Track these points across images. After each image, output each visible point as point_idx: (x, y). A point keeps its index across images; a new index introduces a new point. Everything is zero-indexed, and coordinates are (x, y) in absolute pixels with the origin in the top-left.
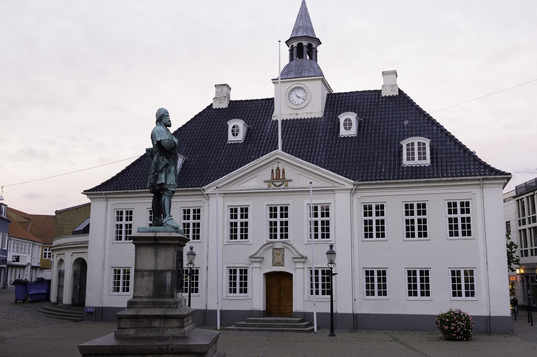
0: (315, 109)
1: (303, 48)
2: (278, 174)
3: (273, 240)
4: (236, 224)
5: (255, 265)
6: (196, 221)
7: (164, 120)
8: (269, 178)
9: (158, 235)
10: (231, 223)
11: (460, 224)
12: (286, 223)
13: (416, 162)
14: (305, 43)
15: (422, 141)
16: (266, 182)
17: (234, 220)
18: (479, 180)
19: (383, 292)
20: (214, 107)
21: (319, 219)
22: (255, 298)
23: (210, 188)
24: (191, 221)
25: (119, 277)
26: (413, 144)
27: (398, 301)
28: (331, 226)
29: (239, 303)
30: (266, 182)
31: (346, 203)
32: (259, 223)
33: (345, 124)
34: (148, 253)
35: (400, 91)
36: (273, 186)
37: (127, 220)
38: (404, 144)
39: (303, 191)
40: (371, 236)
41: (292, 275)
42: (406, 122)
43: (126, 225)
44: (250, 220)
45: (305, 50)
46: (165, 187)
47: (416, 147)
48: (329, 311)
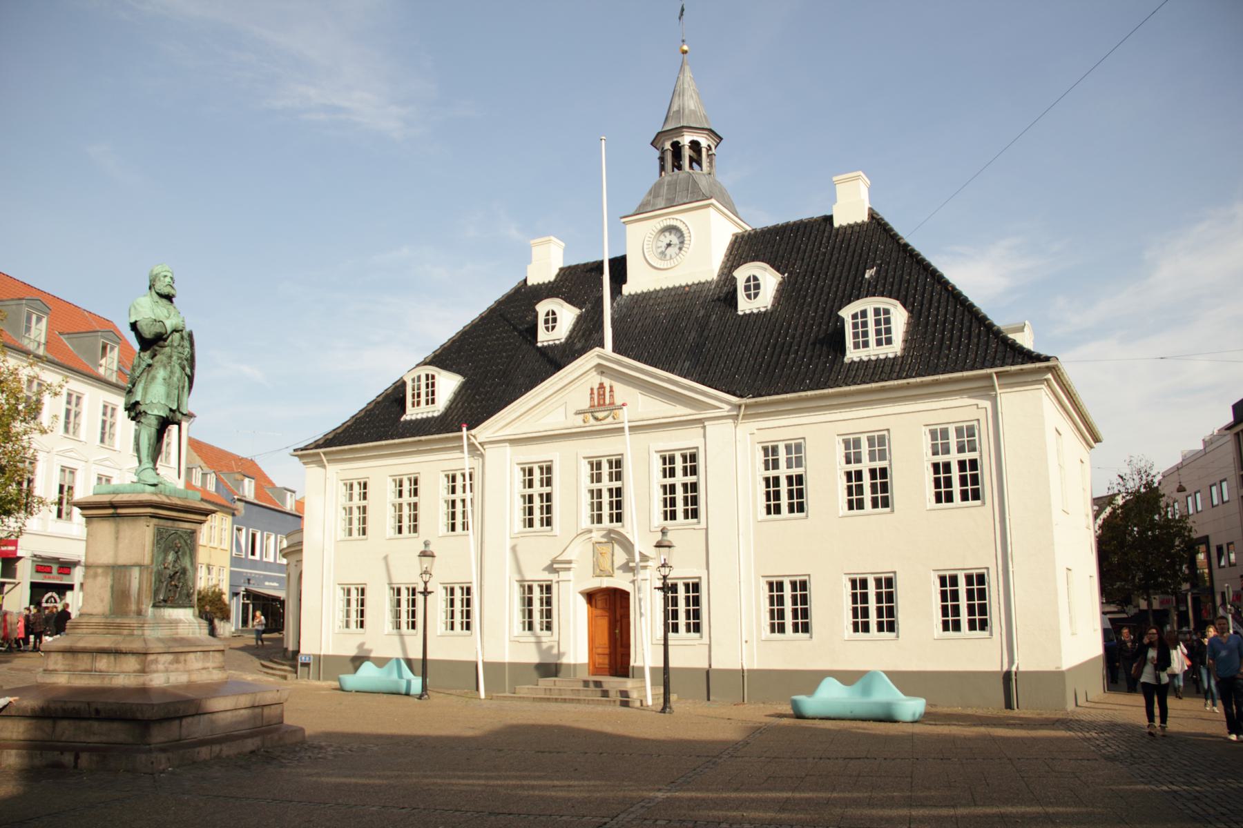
8: (586, 404)
11: (959, 481)
13: (873, 352)
14: (686, 140)
15: (882, 306)
16: (578, 413)
20: (529, 283)
22: (574, 638)
23: (486, 431)
24: (679, 479)
25: (781, 600)
26: (864, 313)
30: (578, 413)
31: (734, 442)
32: (572, 494)
33: (747, 288)
34: (105, 529)
36: (592, 421)
37: (685, 474)
38: (846, 313)
40: (949, 498)
41: (628, 594)
43: (685, 485)
46: (142, 408)
47: (871, 319)
48: (662, 665)
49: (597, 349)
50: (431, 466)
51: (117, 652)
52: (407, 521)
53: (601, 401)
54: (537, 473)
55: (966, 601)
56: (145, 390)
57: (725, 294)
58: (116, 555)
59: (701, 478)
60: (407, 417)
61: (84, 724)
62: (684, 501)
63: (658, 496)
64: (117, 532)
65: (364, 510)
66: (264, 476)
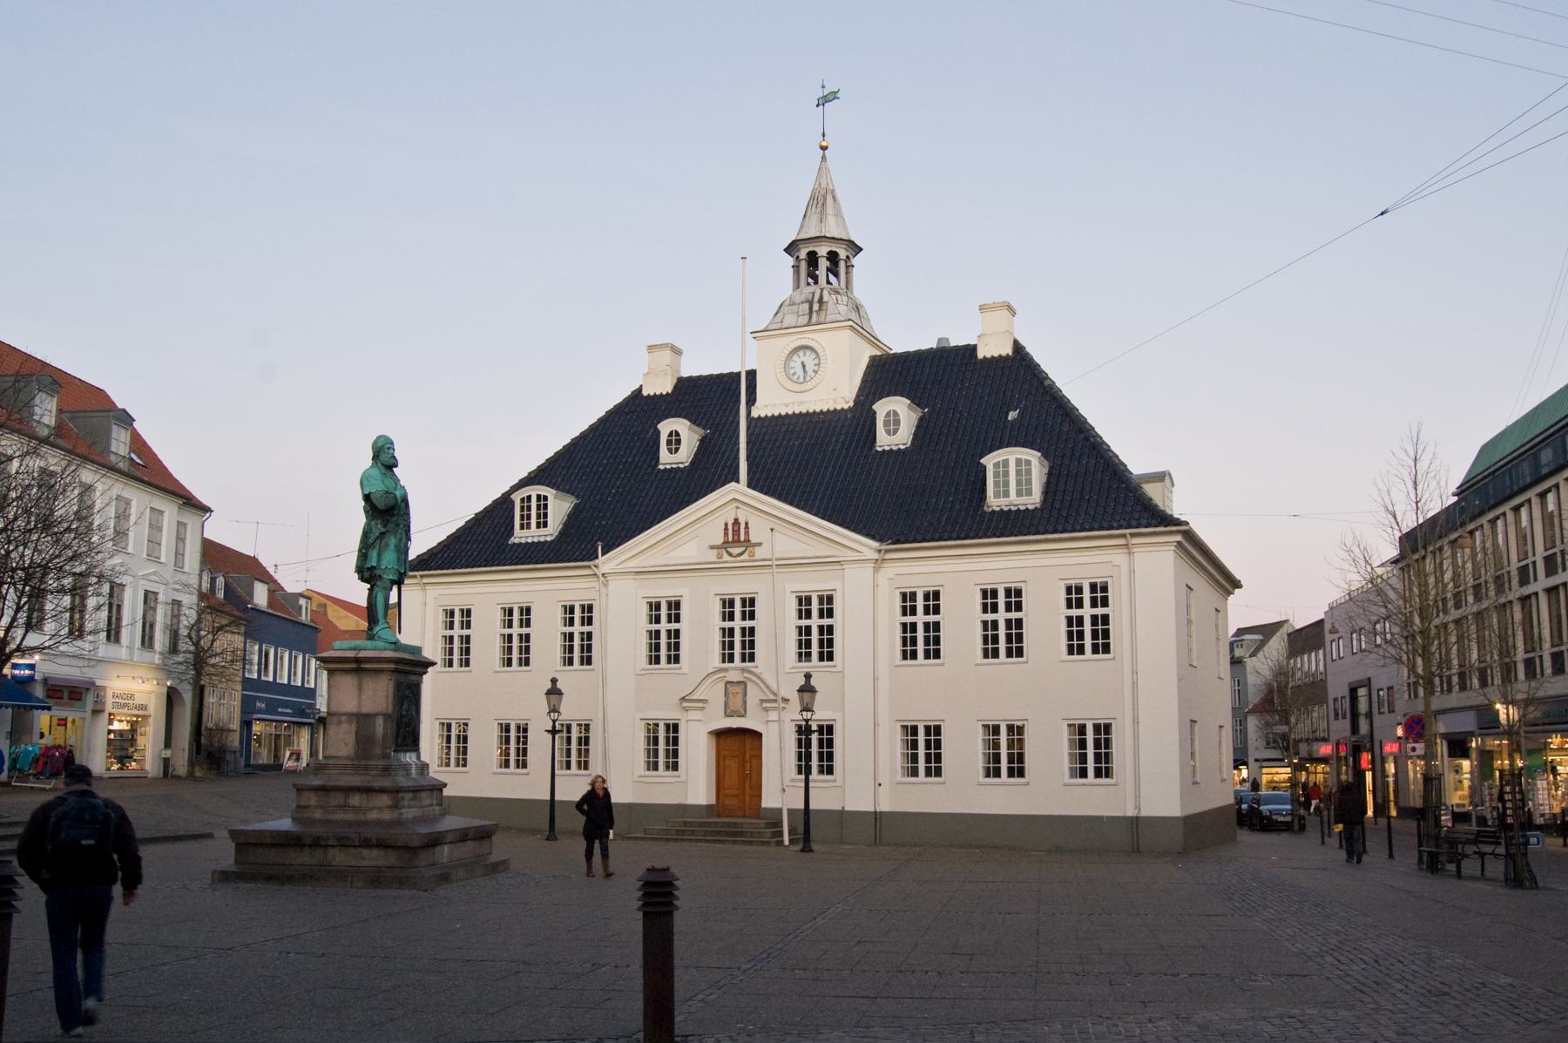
0: (834, 389)
1: (821, 262)
2: (736, 532)
3: (727, 665)
4: (1080, 620)
5: (693, 715)
6: (932, 618)
7: (383, 457)
8: (720, 540)
9: (362, 654)
10: (904, 625)
11: (1090, 632)
12: (1105, 619)
14: (823, 251)
16: (712, 547)
17: (909, 619)
18: (1124, 536)
19: (935, 770)
20: (645, 393)
21: (577, 629)
22: (694, 784)
23: (608, 562)
27: (964, 789)
28: (837, 637)
29: (664, 790)
30: (712, 547)
31: (868, 579)
32: (701, 632)
34: (347, 683)
35: (1018, 347)
36: (726, 557)
37: (744, 619)
38: (990, 461)
39: (788, 564)
42: (1012, 415)
44: (684, 626)
45: (823, 264)
46: (378, 572)
48: (802, 806)
49: (733, 484)
50: (547, 592)
51: (367, 791)
52: (518, 652)
53: (736, 537)
54: (664, 607)
55: (1094, 750)
56: (379, 555)
57: (860, 419)
58: (359, 705)
59: (836, 621)
60: (514, 540)
61: (352, 850)
62: (818, 642)
63: (793, 637)
64: (1138, 808)
65: (526, 638)
66: (275, 581)
